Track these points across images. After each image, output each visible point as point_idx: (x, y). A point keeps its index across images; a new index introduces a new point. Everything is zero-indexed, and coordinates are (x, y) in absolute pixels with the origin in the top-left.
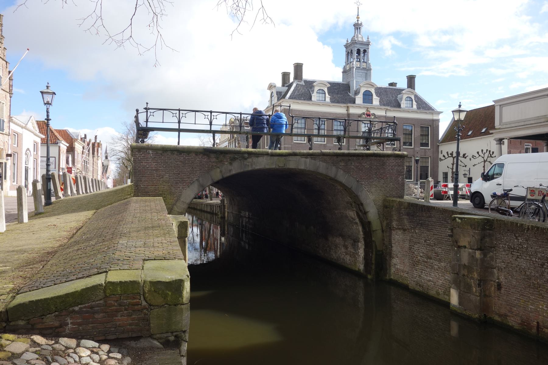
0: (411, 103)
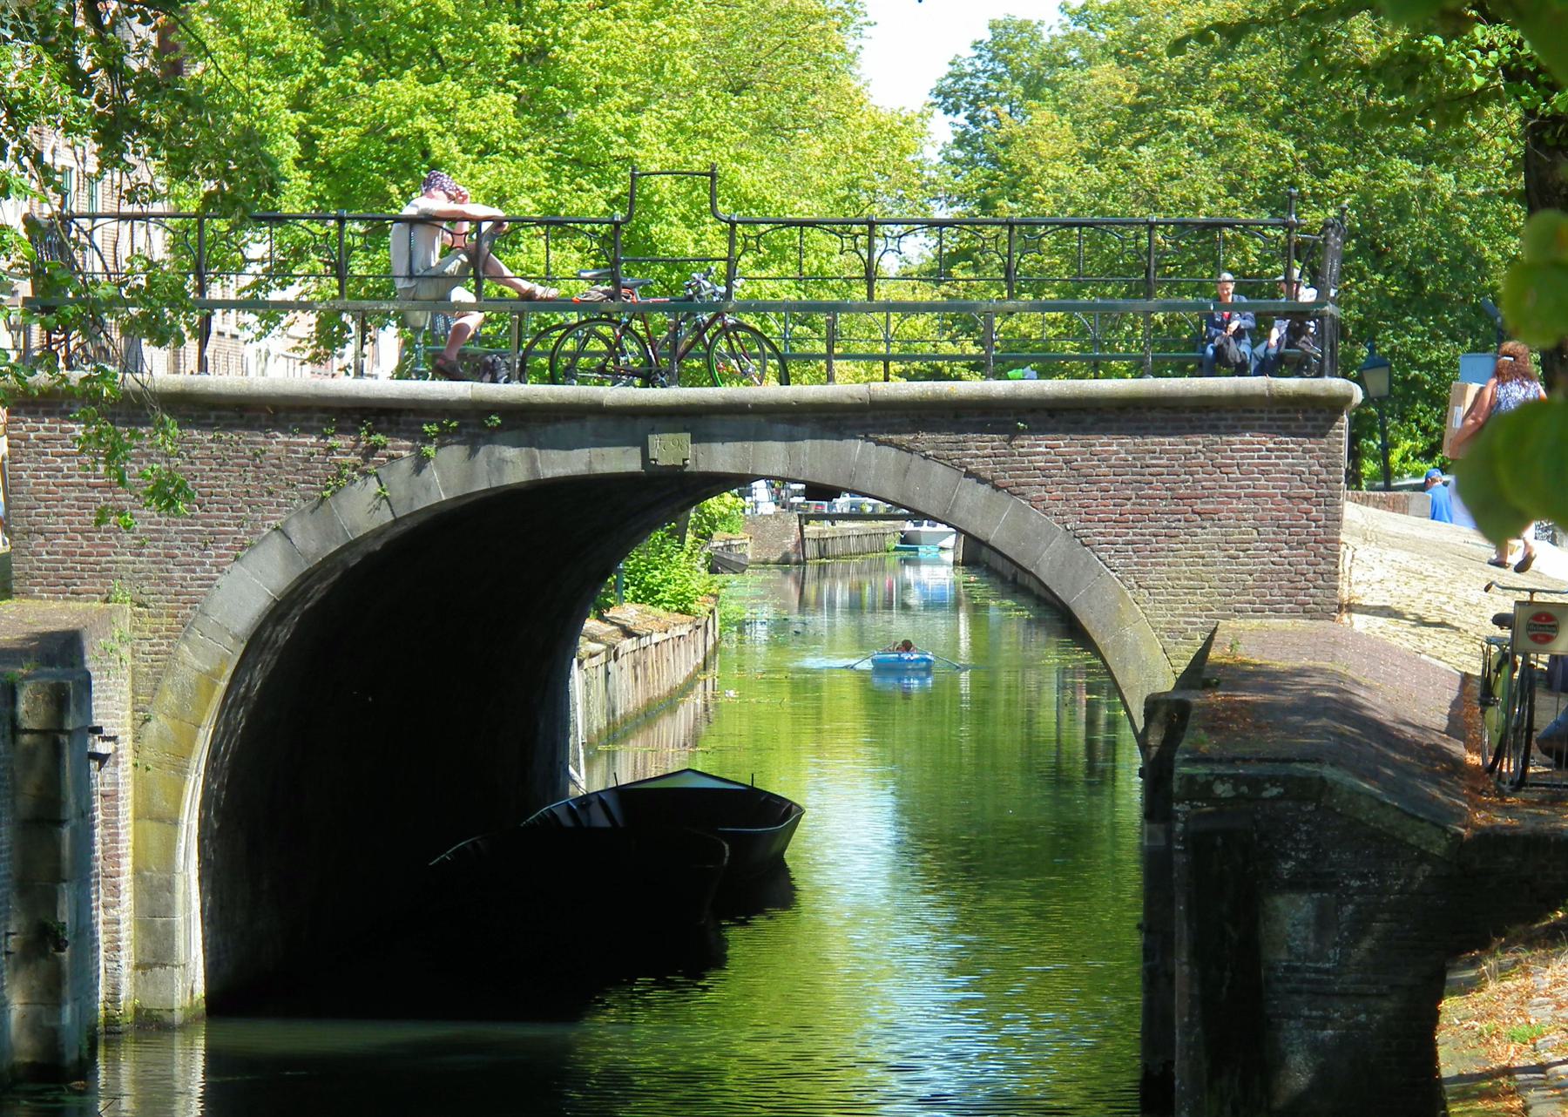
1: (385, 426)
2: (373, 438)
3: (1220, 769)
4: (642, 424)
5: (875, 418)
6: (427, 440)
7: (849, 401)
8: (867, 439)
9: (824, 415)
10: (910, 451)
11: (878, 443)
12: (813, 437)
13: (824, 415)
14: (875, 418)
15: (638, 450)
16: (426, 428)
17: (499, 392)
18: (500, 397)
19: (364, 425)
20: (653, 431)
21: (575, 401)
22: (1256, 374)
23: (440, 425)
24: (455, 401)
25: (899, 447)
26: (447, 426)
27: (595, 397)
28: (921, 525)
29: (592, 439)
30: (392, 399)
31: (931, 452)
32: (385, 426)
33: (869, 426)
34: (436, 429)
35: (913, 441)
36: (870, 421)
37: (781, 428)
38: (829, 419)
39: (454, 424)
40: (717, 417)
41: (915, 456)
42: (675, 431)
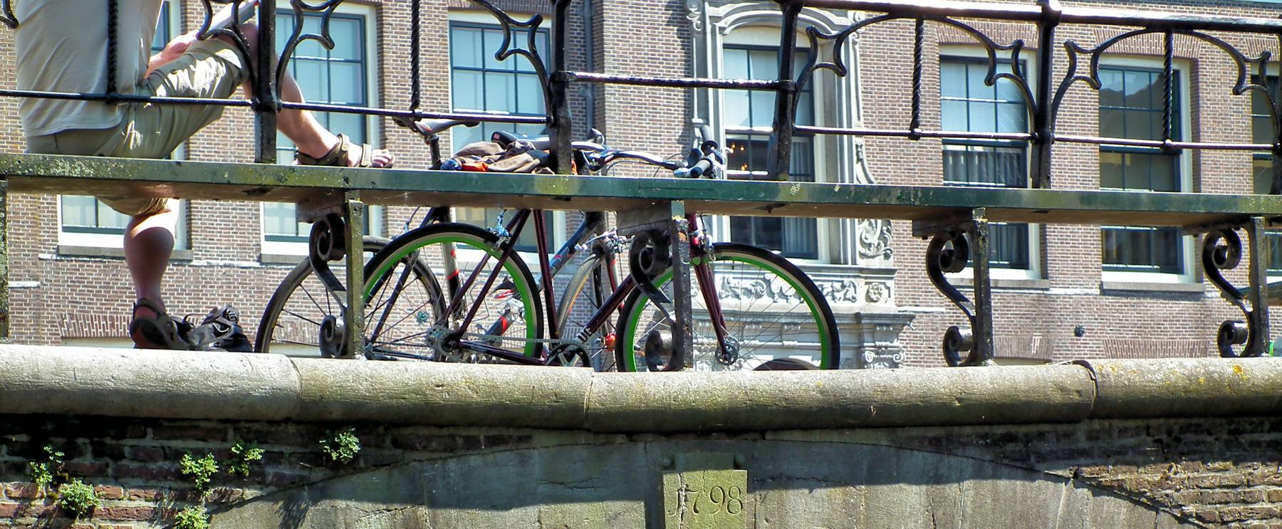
0: (1206, 151)
1: (87, 460)
2: (65, 489)
3: (435, 431)
4: (646, 453)
5: (1092, 436)
6: (188, 491)
7: (1057, 397)
8: (1079, 480)
9: (999, 430)
10: (1154, 505)
11: (1100, 489)
12: (979, 475)
13: (999, 430)
14: (1092, 436)
15: (672, 202)
16: (188, 463)
17: (357, 377)
18: (363, 388)
19: (43, 457)
20: (672, 467)
21: (525, 398)
22: (1269, 432)
23: (223, 457)
24: (263, 399)
25: (1133, 497)
26: (240, 459)
27: (565, 387)
28: (144, 435)
29: (542, 489)
30: (117, 392)
31: (1190, 509)
32: (87, 460)
33: (1084, 453)
34: (212, 467)
35: (1159, 485)
36: (1084, 444)
37: (920, 459)
38: (1011, 438)
39: (256, 454)
40: (797, 436)
41: (1164, 518)
42: (719, 467)
